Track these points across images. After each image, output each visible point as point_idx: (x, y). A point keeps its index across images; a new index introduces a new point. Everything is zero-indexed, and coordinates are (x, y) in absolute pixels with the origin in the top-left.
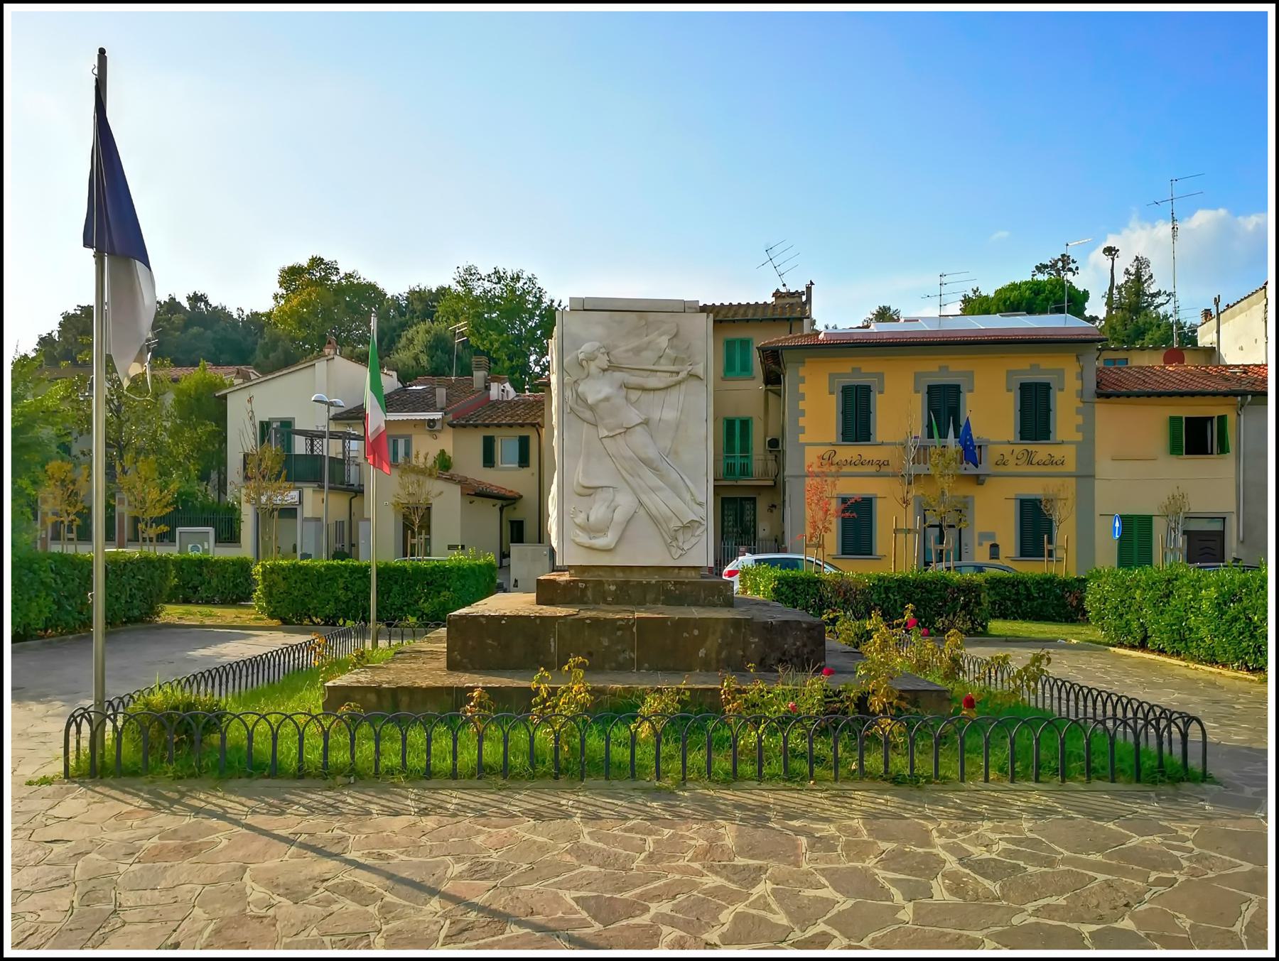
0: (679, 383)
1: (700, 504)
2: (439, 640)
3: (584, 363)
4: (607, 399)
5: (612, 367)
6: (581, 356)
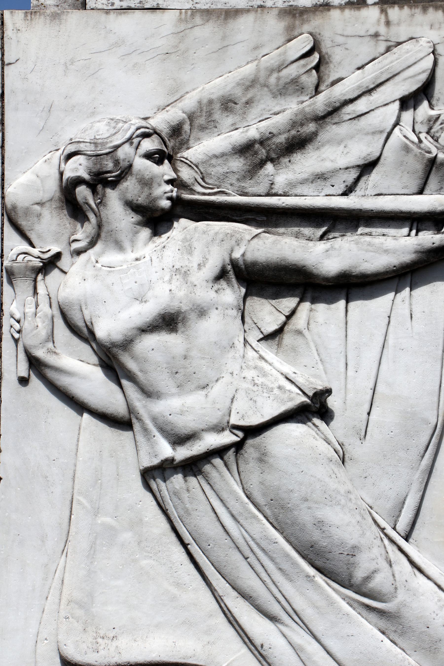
3: (82, 192)
4: (169, 322)
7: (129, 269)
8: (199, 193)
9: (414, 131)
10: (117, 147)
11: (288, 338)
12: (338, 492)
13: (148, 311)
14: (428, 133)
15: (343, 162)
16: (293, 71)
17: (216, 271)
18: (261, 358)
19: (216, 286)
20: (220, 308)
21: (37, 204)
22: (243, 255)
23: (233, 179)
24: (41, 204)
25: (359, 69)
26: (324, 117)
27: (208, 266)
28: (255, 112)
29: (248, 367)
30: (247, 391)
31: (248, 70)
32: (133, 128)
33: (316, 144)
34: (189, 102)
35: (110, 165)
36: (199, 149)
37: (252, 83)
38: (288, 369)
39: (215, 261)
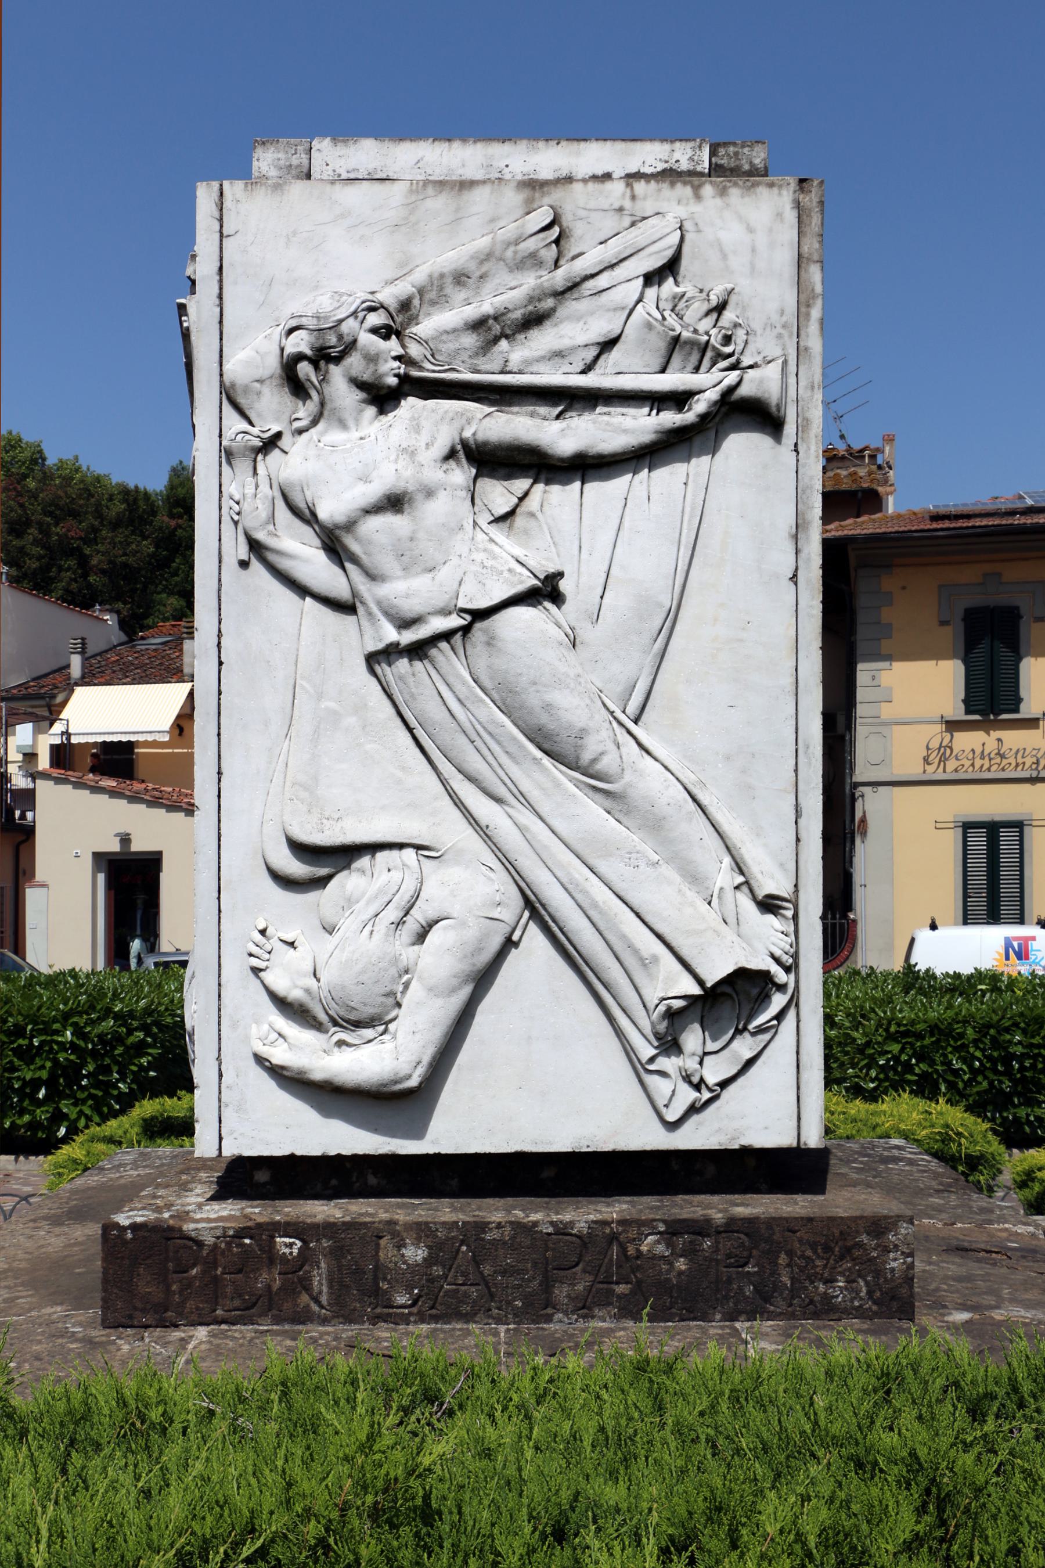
1: (769, 905)
3: (304, 369)
7: (353, 448)
8: (428, 370)
9: (658, 308)
10: (341, 321)
11: (519, 520)
12: (568, 676)
14: (672, 310)
15: (582, 339)
16: (531, 244)
17: (445, 450)
18: (492, 540)
19: (445, 467)
21: (257, 381)
22: (474, 434)
23: (465, 356)
24: (260, 381)
28: (489, 286)
31: (483, 243)
33: (554, 320)
34: (420, 276)
35: (332, 340)
37: (488, 256)
38: (519, 552)
39: (442, 446)
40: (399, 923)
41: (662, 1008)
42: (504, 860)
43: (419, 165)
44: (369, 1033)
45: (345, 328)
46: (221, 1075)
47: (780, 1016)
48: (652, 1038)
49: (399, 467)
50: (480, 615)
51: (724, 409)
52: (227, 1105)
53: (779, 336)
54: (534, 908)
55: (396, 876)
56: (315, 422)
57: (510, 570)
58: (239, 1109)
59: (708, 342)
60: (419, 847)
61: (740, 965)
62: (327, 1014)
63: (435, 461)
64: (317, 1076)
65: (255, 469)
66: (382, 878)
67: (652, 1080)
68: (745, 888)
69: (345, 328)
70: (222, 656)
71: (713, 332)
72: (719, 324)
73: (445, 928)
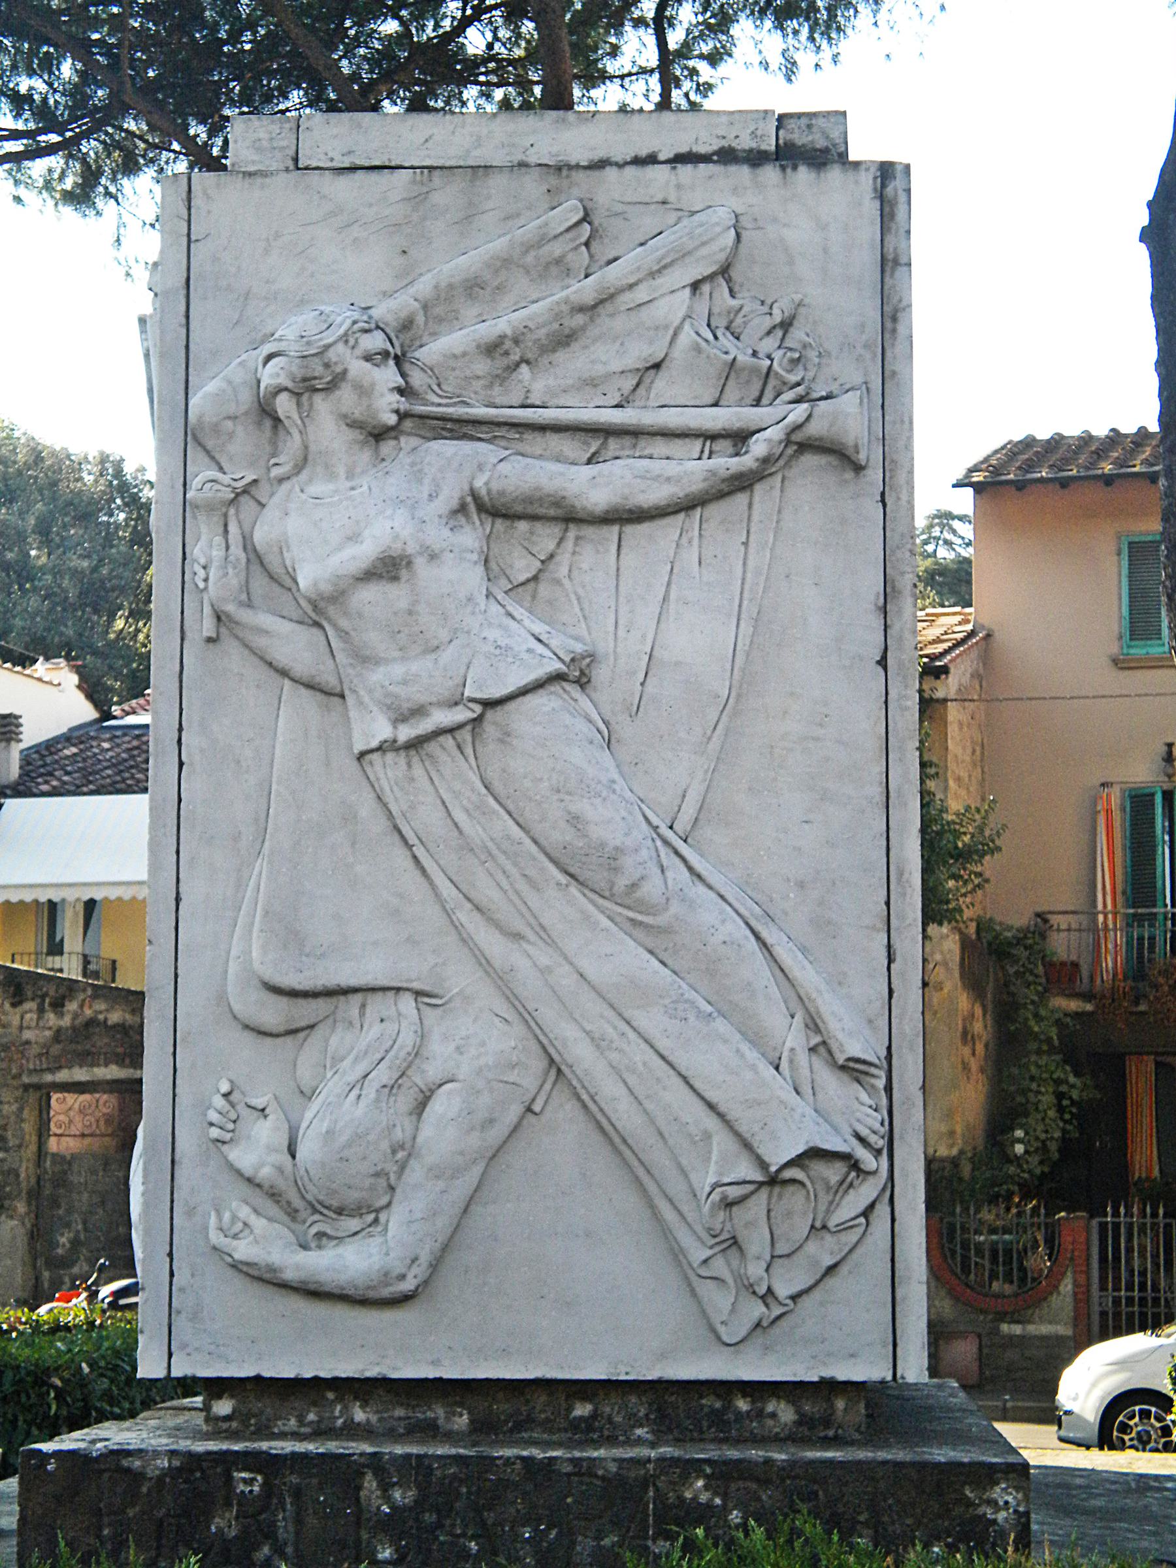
0: (742, 483)
1: (855, 1070)
2: (10, 1514)
3: (284, 405)
4: (389, 568)
5: (424, 422)
6: (271, 375)
7: (341, 501)
8: (433, 404)
9: (709, 325)
10: (327, 347)
11: (544, 589)
12: (599, 782)
13: (365, 552)
14: (727, 328)
15: (616, 365)
16: (556, 249)
17: (455, 504)
18: (510, 615)
19: (452, 523)
20: (456, 550)
21: (229, 418)
22: (486, 484)
23: (478, 385)
24: (234, 418)
25: (642, 244)
26: (594, 307)
27: (441, 498)
28: (508, 300)
29: (490, 624)
30: (488, 656)
31: (499, 245)
32: (348, 322)
33: (583, 341)
34: (424, 286)
35: (319, 370)
36: (432, 351)
37: (505, 263)
38: (539, 628)
39: (450, 495)
40: (391, 1088)
41: (716, 1196)
42: (522, 1010)
43: (428, 145)
44: (354, 1224)
45: (331, 355)
46: (172, 1274)
47: (867, 1212)
48: (704, 1235)
49: (396, 525)
50: (489, 704)
51: (790, 451)
52: (179, 1312)
53: (859, 359)
54: (556, 1068)
55: (391, 1028)
56: (299, 469)
57: (529, 651)
58: (195, 1317)
59: (771, 366)
60: (418, 994)
61: (811, 1144)
62: (303, 1197)
63: (440, 517)
64: (289, 1275)
65: (226, 525)
66: (374, 1031)
67: (707, 1290)
68: (822, 1050)
69: (331, 355)
70: (323, 638)
71: (777, 355)
72: (787, 344)
73: (450, 1093)
